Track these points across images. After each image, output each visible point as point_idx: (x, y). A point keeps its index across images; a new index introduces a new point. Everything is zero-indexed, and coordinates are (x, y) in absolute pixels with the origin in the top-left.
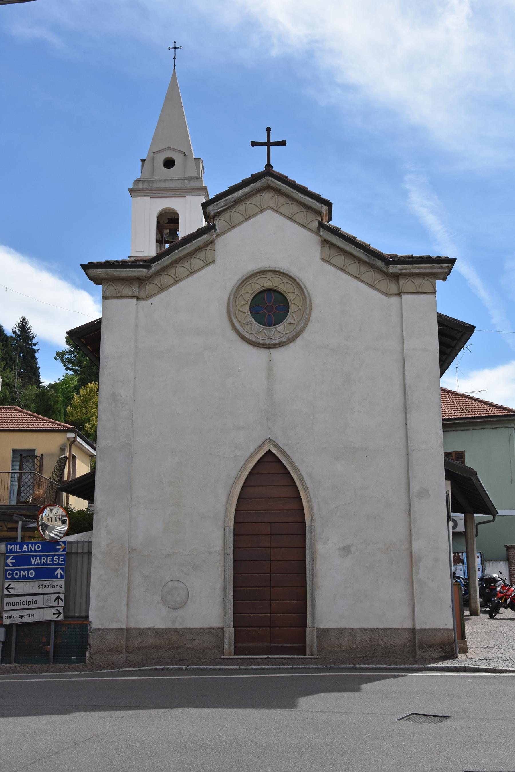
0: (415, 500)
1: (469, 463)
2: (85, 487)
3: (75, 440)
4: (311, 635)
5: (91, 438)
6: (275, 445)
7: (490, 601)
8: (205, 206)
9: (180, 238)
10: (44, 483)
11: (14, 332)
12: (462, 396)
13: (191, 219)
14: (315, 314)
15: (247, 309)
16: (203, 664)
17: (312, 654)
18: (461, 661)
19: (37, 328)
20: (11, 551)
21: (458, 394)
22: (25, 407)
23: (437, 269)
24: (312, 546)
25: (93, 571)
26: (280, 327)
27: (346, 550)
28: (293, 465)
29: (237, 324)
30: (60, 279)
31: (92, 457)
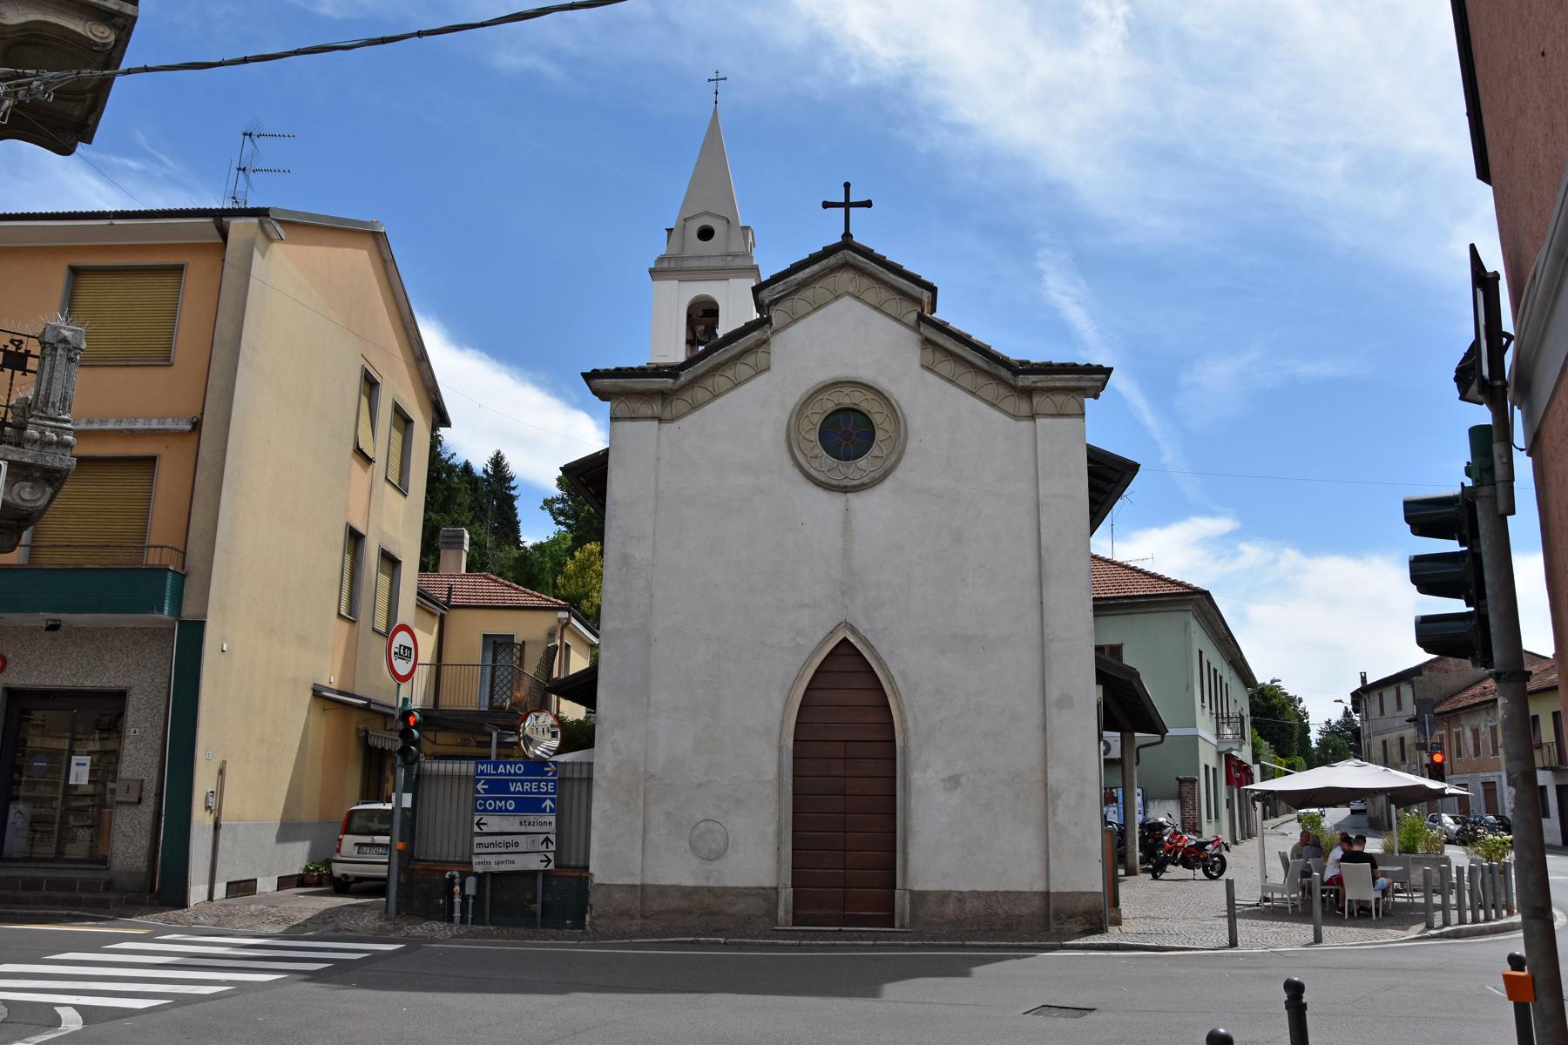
0: (1053, 712)
1: (1128, 660)
2: (583, 688)
3: (568, 622)
4: (902, 901)
5: (592, 620)
6: (854, 631)
7: (1154, 855)
8: (756, 290)
9: (720, 336)
10: (526, 682)
11: (485, 471)
12: (1120, 565)
13: (736, 308)
14: (912, 445)
15: (814, 436)
16: (749, 936)
17: (902, 926)
18: (1113, 936)
19: (516, 465)
20: (482, 773)
21: (1113, 563)
22: (499, 575)
23: (1086, 381)
24: (905, 776)
25: (595, 805)
26: (862, 462)
27: (953, 781)
28: (878, 659)
29: (801, 458)
30: (550, 394)
31: (592, 646)
